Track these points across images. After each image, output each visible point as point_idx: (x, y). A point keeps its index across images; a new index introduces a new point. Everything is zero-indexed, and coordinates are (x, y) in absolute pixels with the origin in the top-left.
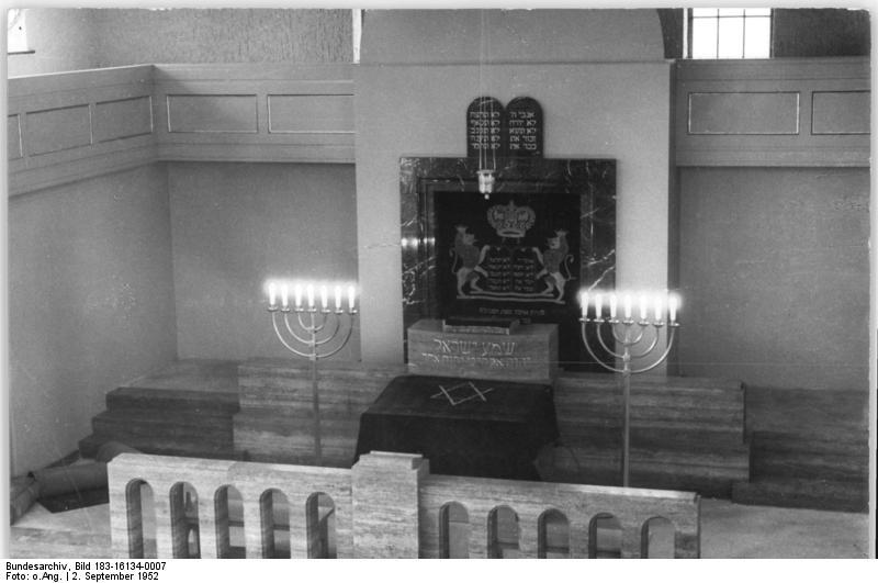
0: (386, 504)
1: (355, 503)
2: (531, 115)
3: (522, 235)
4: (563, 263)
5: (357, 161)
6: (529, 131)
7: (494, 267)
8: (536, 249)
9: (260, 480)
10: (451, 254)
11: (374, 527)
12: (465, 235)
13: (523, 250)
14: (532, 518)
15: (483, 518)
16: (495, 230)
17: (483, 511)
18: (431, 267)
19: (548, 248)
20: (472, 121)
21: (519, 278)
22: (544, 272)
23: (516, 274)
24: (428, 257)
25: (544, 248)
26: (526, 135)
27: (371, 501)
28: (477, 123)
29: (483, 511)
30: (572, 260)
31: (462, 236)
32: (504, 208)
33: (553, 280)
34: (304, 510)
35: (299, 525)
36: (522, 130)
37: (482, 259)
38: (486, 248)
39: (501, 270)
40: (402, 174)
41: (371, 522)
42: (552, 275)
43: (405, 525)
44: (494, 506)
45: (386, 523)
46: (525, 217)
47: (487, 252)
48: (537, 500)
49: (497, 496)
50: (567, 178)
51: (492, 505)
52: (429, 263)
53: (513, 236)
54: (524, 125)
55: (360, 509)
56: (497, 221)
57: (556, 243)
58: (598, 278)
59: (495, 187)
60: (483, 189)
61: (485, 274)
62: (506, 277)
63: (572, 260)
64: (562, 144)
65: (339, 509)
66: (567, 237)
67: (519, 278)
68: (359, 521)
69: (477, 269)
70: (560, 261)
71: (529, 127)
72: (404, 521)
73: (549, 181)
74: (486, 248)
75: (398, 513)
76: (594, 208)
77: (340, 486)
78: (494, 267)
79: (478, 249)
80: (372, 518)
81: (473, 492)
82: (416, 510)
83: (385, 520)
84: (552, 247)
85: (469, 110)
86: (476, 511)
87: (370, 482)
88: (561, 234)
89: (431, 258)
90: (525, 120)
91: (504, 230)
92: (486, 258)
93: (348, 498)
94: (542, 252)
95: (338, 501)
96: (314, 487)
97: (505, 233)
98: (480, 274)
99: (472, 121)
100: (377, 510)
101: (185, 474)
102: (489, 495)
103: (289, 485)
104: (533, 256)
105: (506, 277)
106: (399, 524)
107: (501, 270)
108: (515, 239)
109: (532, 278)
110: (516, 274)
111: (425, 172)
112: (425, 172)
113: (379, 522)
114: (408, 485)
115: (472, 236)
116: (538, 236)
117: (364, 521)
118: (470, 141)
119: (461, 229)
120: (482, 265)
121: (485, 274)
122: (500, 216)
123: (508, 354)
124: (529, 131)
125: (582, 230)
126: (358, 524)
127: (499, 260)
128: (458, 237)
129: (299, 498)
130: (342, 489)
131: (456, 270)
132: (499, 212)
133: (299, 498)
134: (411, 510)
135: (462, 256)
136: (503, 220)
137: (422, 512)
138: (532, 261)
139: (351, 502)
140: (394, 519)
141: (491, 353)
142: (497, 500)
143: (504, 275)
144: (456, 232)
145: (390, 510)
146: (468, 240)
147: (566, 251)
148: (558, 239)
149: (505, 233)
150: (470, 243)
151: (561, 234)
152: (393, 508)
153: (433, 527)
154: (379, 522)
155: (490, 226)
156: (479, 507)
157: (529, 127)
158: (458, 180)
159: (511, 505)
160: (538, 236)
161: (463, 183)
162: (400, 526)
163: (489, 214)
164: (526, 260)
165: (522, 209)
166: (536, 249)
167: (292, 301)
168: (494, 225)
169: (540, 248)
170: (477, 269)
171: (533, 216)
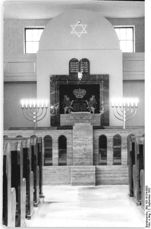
0: (83, 136)
1: (74, 137)
2: (87, 63)
3: (83, 97)
4: (94, 104)
5: (37, 81)
6: (86, 67)
7: (75, 106)
8: (86, 101)
9: (44, 133)
10: (62, 103)
11: (79, 143)
12: (67, 98)
13: (83, 101)
14: (125, 137)
15: (111, 139)
16: (75, 96)
17: (111, 136)
18: (58, 106)
19: (90, 100)
20: (71, 65)
21: (82, 109)
22: (89, 107)
23: (81, 108)
24: (58, 103)
25: (89, 101)
26: (85, 68)
27: (78, 135)
28: (72, 65)
29: (111, 136)
30: (96, 103)
31: (66, 98)
32: (78, 90)
33: (91, 109)
34: (57, 141)
35: (56, 145)
36: (84, 67)
37: (72, 104)
38: (73, 101)
39: (77, 109)
40: (51, 80)
41: (78, 142)
42: (91, 108)
43: (89, 142)
44: (114, 135)
45: (83, 142)
46: (84, 92)
47: (73, 102)
48: (127, 132)
49: (115, 132)
50: (96, 79)
51: (114, 134)
52: (58, 105)
53: (80, 97)
54: (85, 66)
55: (75, 138)
56: (76, 93)
57: (92, 99)
58: (62, 149)
59: (83, 77)
60: (79, 77)
61: (72, 108)
62: (78, 109)
63: (96, 103)
64: (95, 70)
65: (68, 139)
66: (95, 97)
67: (82, 109)
68: (75, 142)
69: (70, 107)
70: (93, 104)
71: (86, 66)
72: (88, 141)
73: (91, 80)
74: (73, 101)
75: (87, 138)
76: (104, 87)
77: (68, 133)
78: (75, 106)
79: (70, 101)
80: (79, 141)
81: (109, 131)
82: (92, 137)
83: (83, 141)
84: (91, 100)
85: (70, 62)
86: (109, 136)
87: (78, 130)
88: (93, 96)
89: (58, 103)
90: (85, 64)
91: (78, 96)
92: (73, 104)
93: (72, 136)
94: (88, 102)
95: (68, 137)
96: (61, 133)
97: (78, 97)
98: (71, 108)
99: (71, 65)
100: (80, 138)
101: (20, 133)
102: (113, 132)
103: (53, 134)
104: (86, 103)
105: (78, 109)
106: (87, 142)
107: (77, 109)
108: (81, 98)
109: (85, 109)
110: (81, 108)
111: (57, 79)
112: (57, 79)
113: (80, 142)
114: (90, 130)
115: (69, 98)
116: (87, 97)
117: (77, 142)
118: (70, 70)
119: (65, 96)
120: (71, 106)
121: (72, 108)
122: (77, 92)
123: (90, 119)
124: (86, 67)
125: (100, 94)
126: (74, 143)
127: (76, 104)
128: (65, 98)
129: (56, 138)
130: (69, 133)
131: (64, 108)
132: (77, 91)
133: (56, 138)
134: (91, 137)
135: (66, 103)
136: (77, 93)
137: (94, 138)
138: (85, 104)
139: (72, 137)
140: (85, 140)
141: (86, 119)
142: (115, 133)
143: (78, 108)
144: (64, 97)
145: (84, 138)
146: (68, 99)
147: (95, 101)
148: (92, 98)
149: (78, 97)
150: (68, 100)
151: (93, 96)
152: (85, 137)
153: (97, 142)
154: (80, 142)
155: (74, 95)
156: (110, 135)
157: (86, 66)
158: (66, 81)
159: (119, 134)
160: (87, 97)
161: (68, 82)
162: (88, 142)
163: (74, 92)
164: (83, 104)
165: (82, 90)
166: (86, 101)
167: (29, 105)
168: (75, 94)
169: (87, 100)
170: (70, 107)
171: (86, 92)
